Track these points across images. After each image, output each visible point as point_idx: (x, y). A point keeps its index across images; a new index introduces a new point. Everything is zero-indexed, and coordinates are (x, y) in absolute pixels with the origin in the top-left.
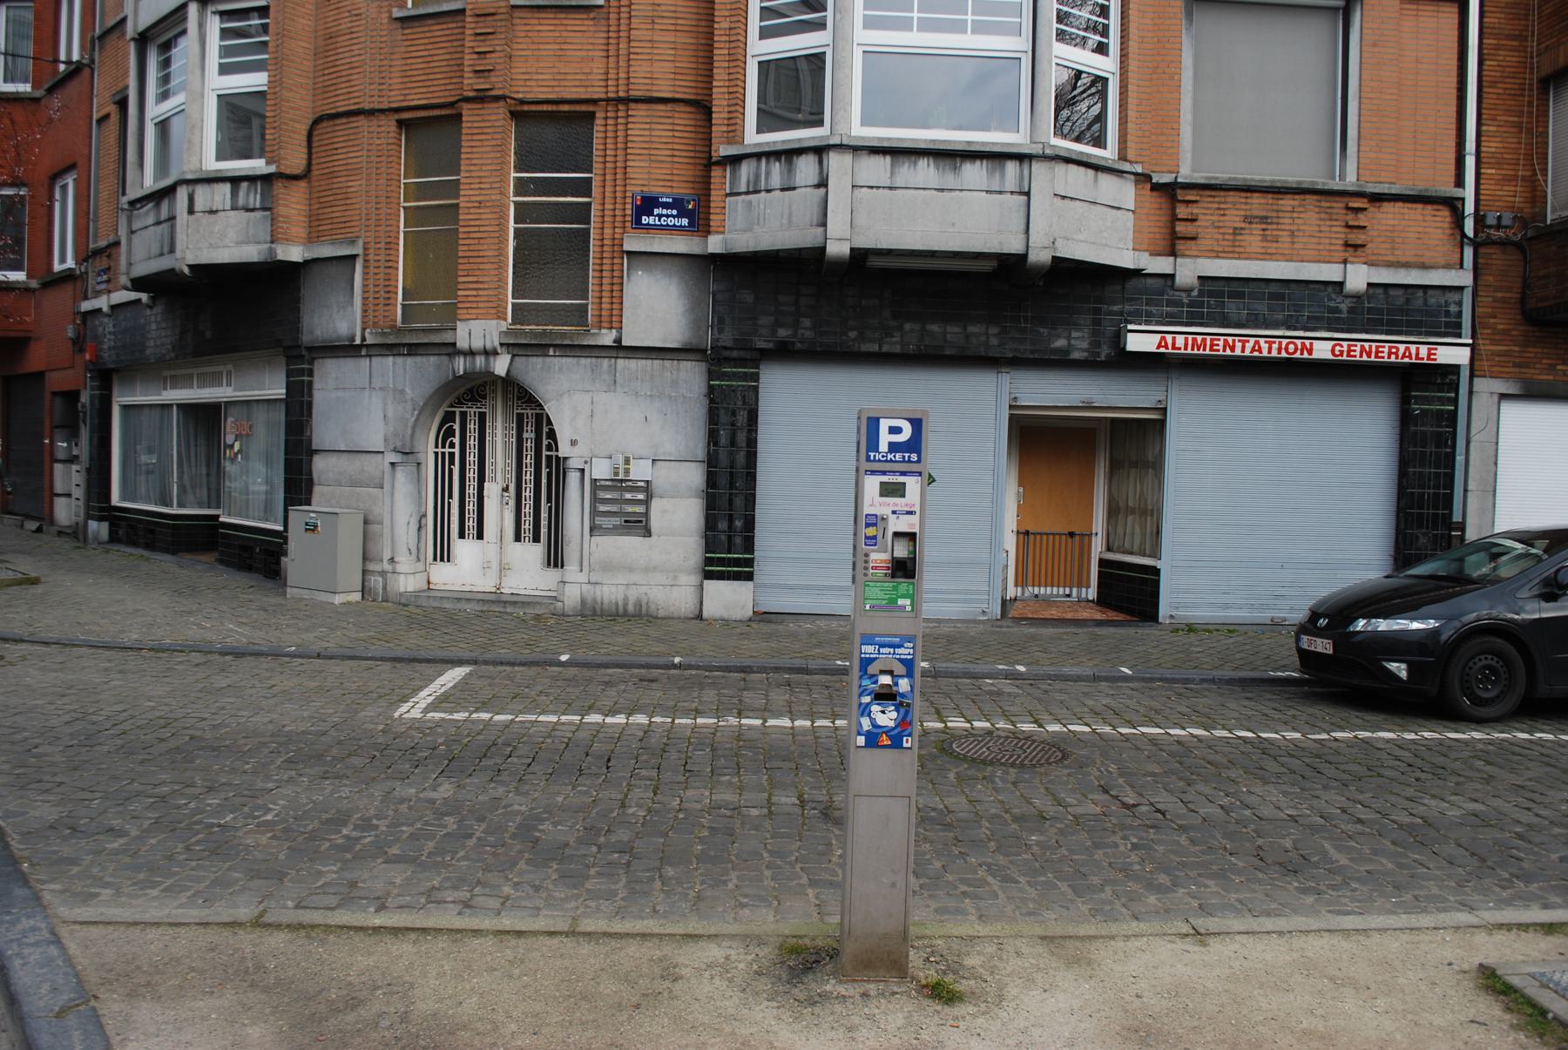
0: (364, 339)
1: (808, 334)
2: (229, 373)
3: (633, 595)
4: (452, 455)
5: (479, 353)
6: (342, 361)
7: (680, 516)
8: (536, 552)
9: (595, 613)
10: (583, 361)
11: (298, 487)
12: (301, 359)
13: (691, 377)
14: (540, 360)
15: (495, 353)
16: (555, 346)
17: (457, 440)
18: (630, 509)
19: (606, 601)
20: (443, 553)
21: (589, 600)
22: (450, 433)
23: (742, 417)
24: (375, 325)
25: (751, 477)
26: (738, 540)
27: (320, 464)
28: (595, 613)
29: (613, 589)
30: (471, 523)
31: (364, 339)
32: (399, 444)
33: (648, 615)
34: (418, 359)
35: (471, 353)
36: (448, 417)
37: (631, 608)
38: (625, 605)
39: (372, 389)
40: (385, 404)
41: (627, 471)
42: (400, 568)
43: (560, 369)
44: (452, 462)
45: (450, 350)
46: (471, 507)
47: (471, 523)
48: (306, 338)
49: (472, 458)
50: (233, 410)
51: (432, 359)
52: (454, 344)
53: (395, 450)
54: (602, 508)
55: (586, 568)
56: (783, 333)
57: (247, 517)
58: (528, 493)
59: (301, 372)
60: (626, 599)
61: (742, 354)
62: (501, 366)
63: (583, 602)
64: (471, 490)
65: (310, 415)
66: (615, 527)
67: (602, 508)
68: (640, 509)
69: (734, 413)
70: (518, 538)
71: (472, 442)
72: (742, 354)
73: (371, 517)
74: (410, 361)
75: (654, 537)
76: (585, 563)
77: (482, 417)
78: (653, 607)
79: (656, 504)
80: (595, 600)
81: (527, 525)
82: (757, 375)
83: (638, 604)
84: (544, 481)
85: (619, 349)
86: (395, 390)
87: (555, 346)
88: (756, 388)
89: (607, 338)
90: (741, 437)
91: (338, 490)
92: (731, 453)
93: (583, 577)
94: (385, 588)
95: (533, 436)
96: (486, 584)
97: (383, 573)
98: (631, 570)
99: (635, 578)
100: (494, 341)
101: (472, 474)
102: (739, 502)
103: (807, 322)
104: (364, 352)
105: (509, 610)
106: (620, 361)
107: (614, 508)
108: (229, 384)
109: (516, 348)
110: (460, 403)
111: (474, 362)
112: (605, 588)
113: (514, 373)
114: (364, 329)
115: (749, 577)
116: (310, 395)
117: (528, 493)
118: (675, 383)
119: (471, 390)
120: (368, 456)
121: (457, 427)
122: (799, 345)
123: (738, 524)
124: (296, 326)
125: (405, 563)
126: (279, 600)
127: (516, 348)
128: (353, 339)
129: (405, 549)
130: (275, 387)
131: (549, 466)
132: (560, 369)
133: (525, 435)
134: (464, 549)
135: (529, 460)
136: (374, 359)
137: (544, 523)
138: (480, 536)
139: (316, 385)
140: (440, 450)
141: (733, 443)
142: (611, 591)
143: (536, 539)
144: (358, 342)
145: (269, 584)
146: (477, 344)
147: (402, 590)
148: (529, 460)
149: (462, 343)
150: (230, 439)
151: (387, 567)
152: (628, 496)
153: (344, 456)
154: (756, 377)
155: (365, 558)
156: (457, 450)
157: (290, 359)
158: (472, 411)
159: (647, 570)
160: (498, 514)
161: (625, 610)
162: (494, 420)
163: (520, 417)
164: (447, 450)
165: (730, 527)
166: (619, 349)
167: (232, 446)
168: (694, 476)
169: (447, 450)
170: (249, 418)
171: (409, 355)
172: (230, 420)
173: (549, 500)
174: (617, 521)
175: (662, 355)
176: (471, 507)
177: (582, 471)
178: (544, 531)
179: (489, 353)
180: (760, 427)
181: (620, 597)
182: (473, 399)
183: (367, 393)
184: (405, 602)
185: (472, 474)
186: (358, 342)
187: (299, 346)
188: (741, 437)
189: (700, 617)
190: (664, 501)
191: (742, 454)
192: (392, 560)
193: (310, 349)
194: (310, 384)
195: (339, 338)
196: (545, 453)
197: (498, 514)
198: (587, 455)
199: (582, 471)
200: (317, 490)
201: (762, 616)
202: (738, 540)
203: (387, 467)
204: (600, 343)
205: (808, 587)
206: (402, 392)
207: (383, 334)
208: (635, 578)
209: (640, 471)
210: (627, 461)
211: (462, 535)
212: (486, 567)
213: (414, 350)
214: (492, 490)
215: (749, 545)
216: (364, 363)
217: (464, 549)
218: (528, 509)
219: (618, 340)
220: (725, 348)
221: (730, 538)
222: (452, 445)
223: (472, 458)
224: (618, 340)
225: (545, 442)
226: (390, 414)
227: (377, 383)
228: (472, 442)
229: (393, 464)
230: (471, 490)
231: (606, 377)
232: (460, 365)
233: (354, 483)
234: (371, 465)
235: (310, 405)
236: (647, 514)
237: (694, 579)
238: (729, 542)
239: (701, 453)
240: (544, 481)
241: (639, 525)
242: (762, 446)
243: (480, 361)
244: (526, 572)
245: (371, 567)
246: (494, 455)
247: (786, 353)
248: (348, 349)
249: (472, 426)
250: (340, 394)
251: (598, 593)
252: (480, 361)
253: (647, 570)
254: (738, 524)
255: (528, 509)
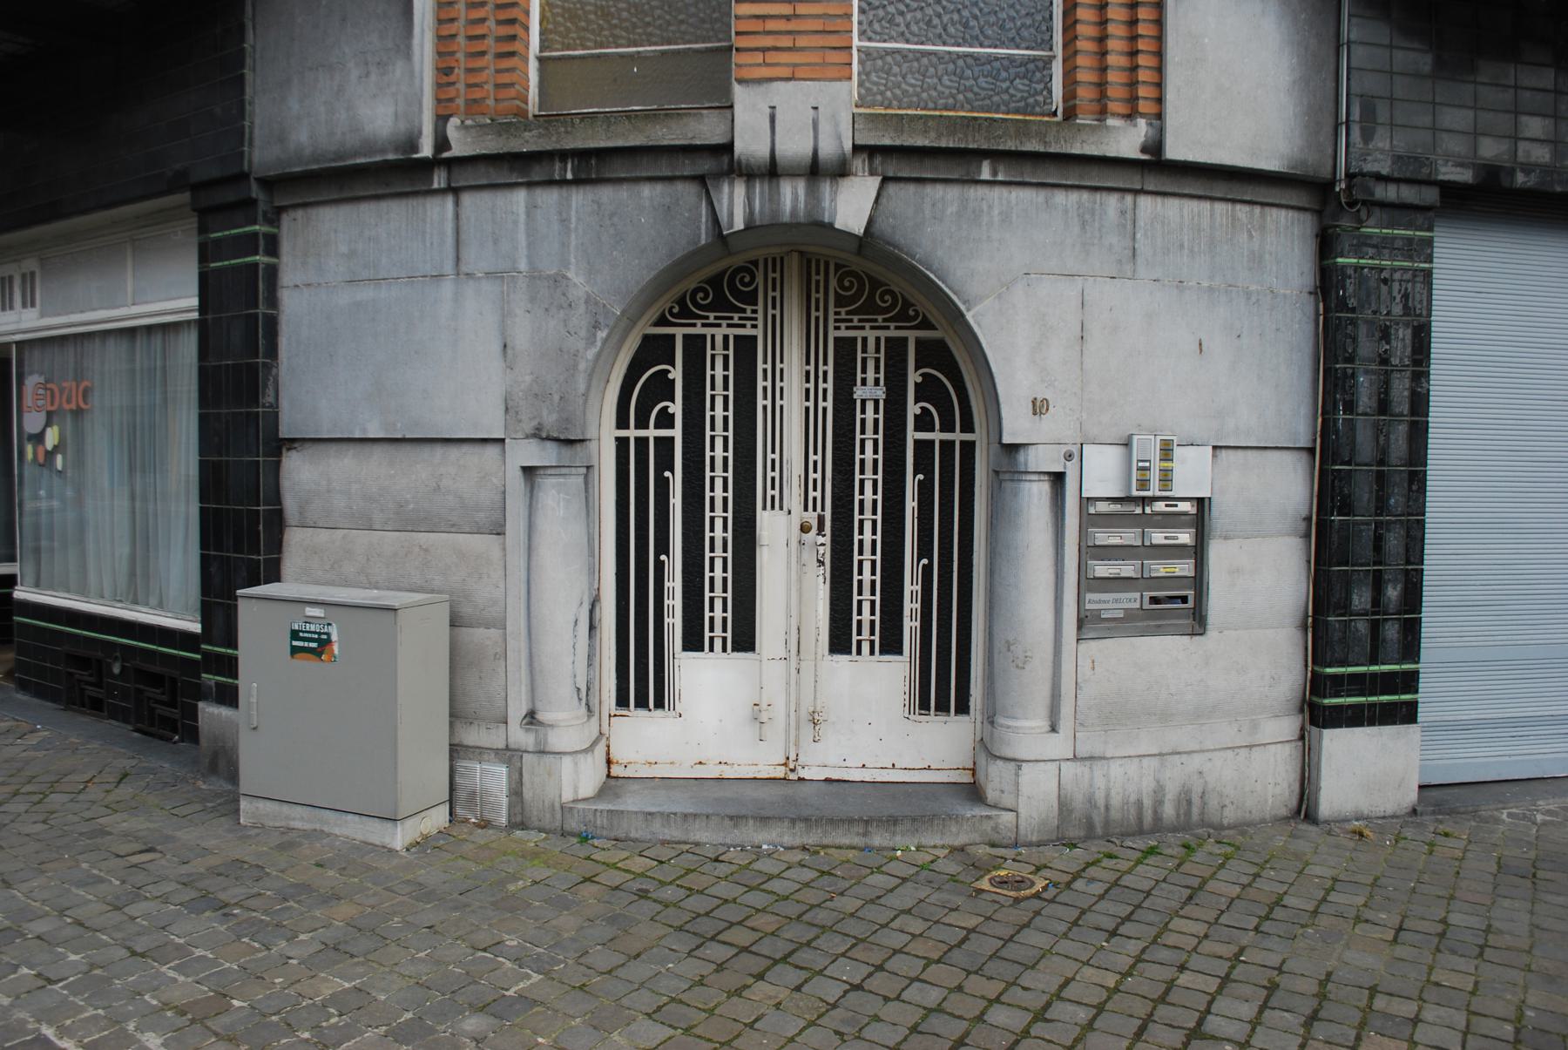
0: (442, 143)
1: (1541, 154)
2: (28, 279)
3: (1175, 776)
4: (665, 445)
5: (793, 173)
6: (367, 210)
7: (1262, 576)
8: (889, 677)
9: (1090, 834)
10: (1060, 197)
11: (241, 534)
12: (239, 213)
13: (1281, 243)
14: (953, 192)
15: (841, 171)
16: (996, 156)
17: (676, 408)
18: (1160, 569)
19: (1116, 801)
20: (643, 684)
21: (1078, 801)
22: (662, 387)
23: (1403, 336)
24: (473, 106)
25: (1417, 481)
26: (1392, 631)
27: (301, 475)
28: (1090, 834)
29: (1132, 767)
30: (718, 613)
31: (442, 143)
32: (550, 420)
33: (1203, 823)
34: (606, 193)
35: (773, 171)
36: (654, 350)
37: (1169, 811)
38: (1158, 803)
39: (460, 272)
40: (505, 316)
41: (1166, 478)
42: (557, 740)
43: (1006, 218)
44: (665, 462)
45: (705, 165)
46: (718, 572)
47: (718, 613)
48: (263, 155)
49: (719, 451)
50: (35, 357)
51: (646, 190)
52: (728, 148)
53: (539, 435)
54: (1102, 570)
55: (1066, 723)
56: (1490, 150)
57: (83, 592)
58: (868, 534)
59: (249, 244)
60: (1159, 791)
61: (1408, 194)
62: (852, 205)
63: (1064, 806)
64: (719, 532)
65: (273, 351)
66: (1130, 616)
67: (1102, 570)
68: (1184, 568)
69: (1385, 335)
70: (840, 642)
71: (719, 412)
72: (1408, 194)
73: (466, 610)
74: (579, 199)
75: (1212, 633)
76: (1066, 709)
77: (745, 347)
78: (1213, 803)
79: (1217, 552)
80: (1091, 801)
81: (866, 614)
82: (1429, 243)
83: (1185, 800)
84: (911, 504)
85: (1158, 170)
86: (534, 276)
87: (996, 156)
88: (1428, 274)
89: (1127, 140)
90: (1400, 389)
91: (362, 538)
92: (1378, 430)
93: (1058, 745)
94: (516, 792)
95: (880, 393)
96: (762, 760)
97: (509, 755)
98: (1165, 717)
99: (1179, 737)
100: (836, 139)
101: (719, 491)
102: (1394, 541)
103: (1535, 126)
104: (439, 180)
105: (878, 839)
106: (1145, 202)
107: (1127, 569)
108: (29, 302)
109: (897, 159)
110: (684, 310)
111: (774, 197)
112: (1116, 770)
113: (883, 225)
114: (441, 120)
115: (1407, 714)
116: (273, 301)
117: (868, 534)
118: (1256, 260)
119: (715, 281)
120: (454, 452)
121: (676, 374)
122: (1520, 179)
123: (1393, 593)
124: (233, 125)
125: (567, 726)
126: (208, 839)
127: (897, 159)
128: (413, 145)
129: (566, 691)
130: (167, 292)
131: (923, 464)
132: (1006, 218)
133: (859, 393)
134: (703, 678)
135: (869, 453)
136: (467, 199)
137: (911, 606)
138: (744, 640)
139: (287, 277)
140: (632, 433)
141: (1384, 406)
142: (1126, 777)
143: (891, 644)
144: (426, 150)
145: (162, 762)
146: (794, 146)
147: (567, 796)
148: (869, 453)
149: (750, 144)
150: (33, 422)
151: (519, 736)
152: (1158, 537)
153: (378, 452)
154: (1424, 249)
155: (457, 715)
156: (677, 433)
157: (207, 215)
158: (719, 333)
159: (1200, 715)
160: (790, 575)
161: (1157, 817)
162: (777, 355)
163: (846, 353)
164: (652, 433)
165: (1376, 601)
166: (1158, 170)
167: (39, 438)
168: (1287, 487)
169: (652, 433)
170: (79, 375)
171: (577, 182)
172: (32, 381)
173: (924, 549)
174: (1131, 600)
175: (1238, 191)
176: (718, 572)
177: (1058, 479)
178: (911, 625)
179: (816, 171)
180: (1435, 369)
181: (1148, 785)
182: (721, 305)
183: (447, 288)
184: (576, 833)
185: (719, 491)
186: (426, 150)
187: (243, 177)
188: (1400, 389)
189: (1305, 808)
190: (1232, 545)
191: (1402, 429)
192: (531, 717)
193: (268, 184)
194: (273, 273)
195: (369, 146)
196: (912, 435)
197: (790, 575)
198: (1070, 434)
199: (1058, 479)
200: (294, 538)
201: (1438, 797)
202: (1392, 631)
203: (516, 480)
204: (1112, 152)
205: (1495, 724)
206: (558, 280)
207: (504, 129)
208: (1179, 737)
209: (1193, 474)
210: (1167, 452)
211: (693, 641)
212: (757, 715)
213: (593, 166)
214: (775, 530)
215: (1411, 646)
216: (440, 210)
217: (703, 678)
218: (867, 574)
219: (1155, 147)
220: (1379, 177)
221: (1375, 627)
222: (666, 420)
223: (719, 451)
224: (1155, 147)
225: (913, 409)
226: (521, 337)
227: (478, 259)
228: (719, 412)
229: (529, 471)
230: (719, 532)
231: (1113, 239)
232: (736, 204)
233: (412, 521)
234: (466, 475)
235: (272, 325)
236: (1199, 581)
237: (1288, 726)
238: (1361, 647)
239: (1299, 424)
240: (911, 504)
241: (1183, 607)
242: (1437, 415)
243: (791, 196)
244: (869, 722)
245: (472, 736)
246: (777, 442)
247: (1493, 200)
248: (399, 174)
249: (718, 372)
250: (366, 294)
251: (1100, 783)
252: (791, 196)
253: (1200, 715)
254: (1393, 593)
255: (867, 574)
